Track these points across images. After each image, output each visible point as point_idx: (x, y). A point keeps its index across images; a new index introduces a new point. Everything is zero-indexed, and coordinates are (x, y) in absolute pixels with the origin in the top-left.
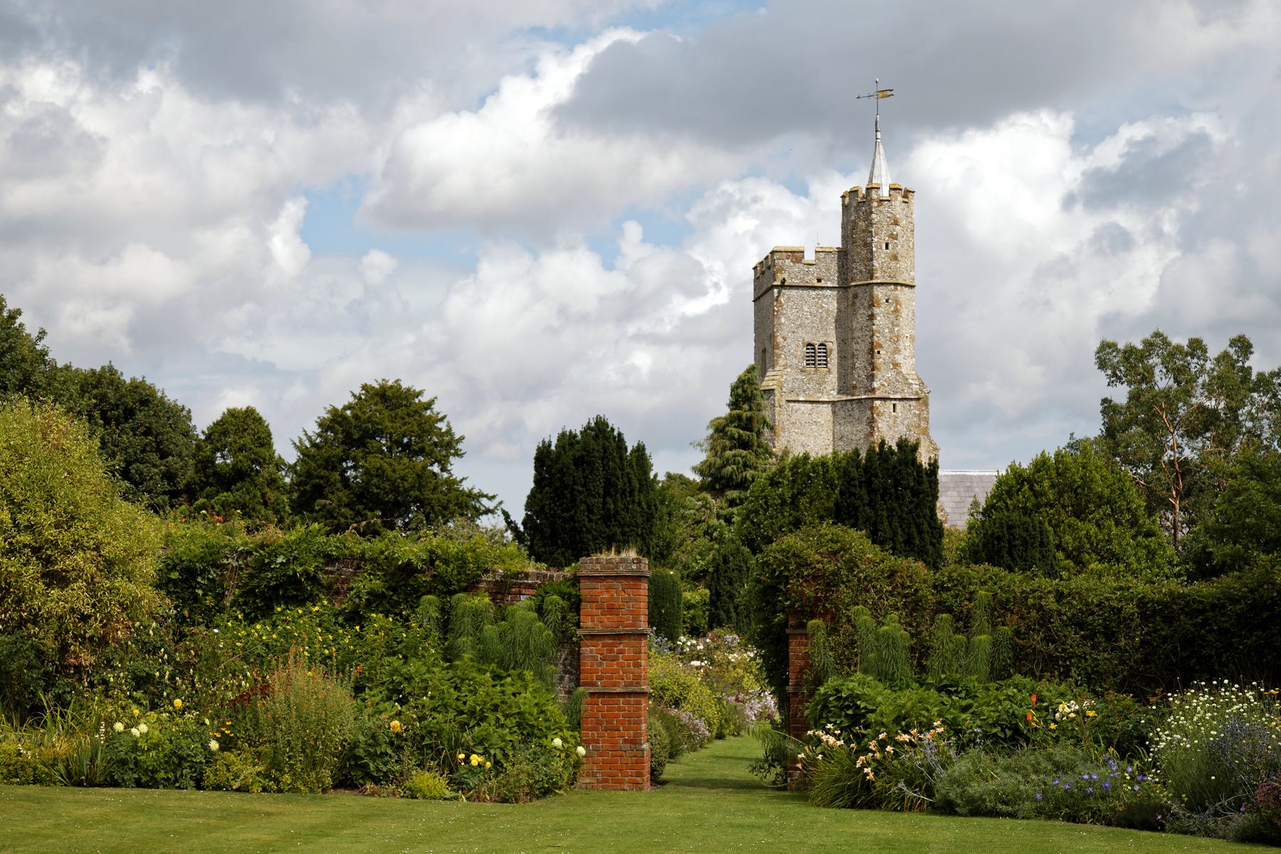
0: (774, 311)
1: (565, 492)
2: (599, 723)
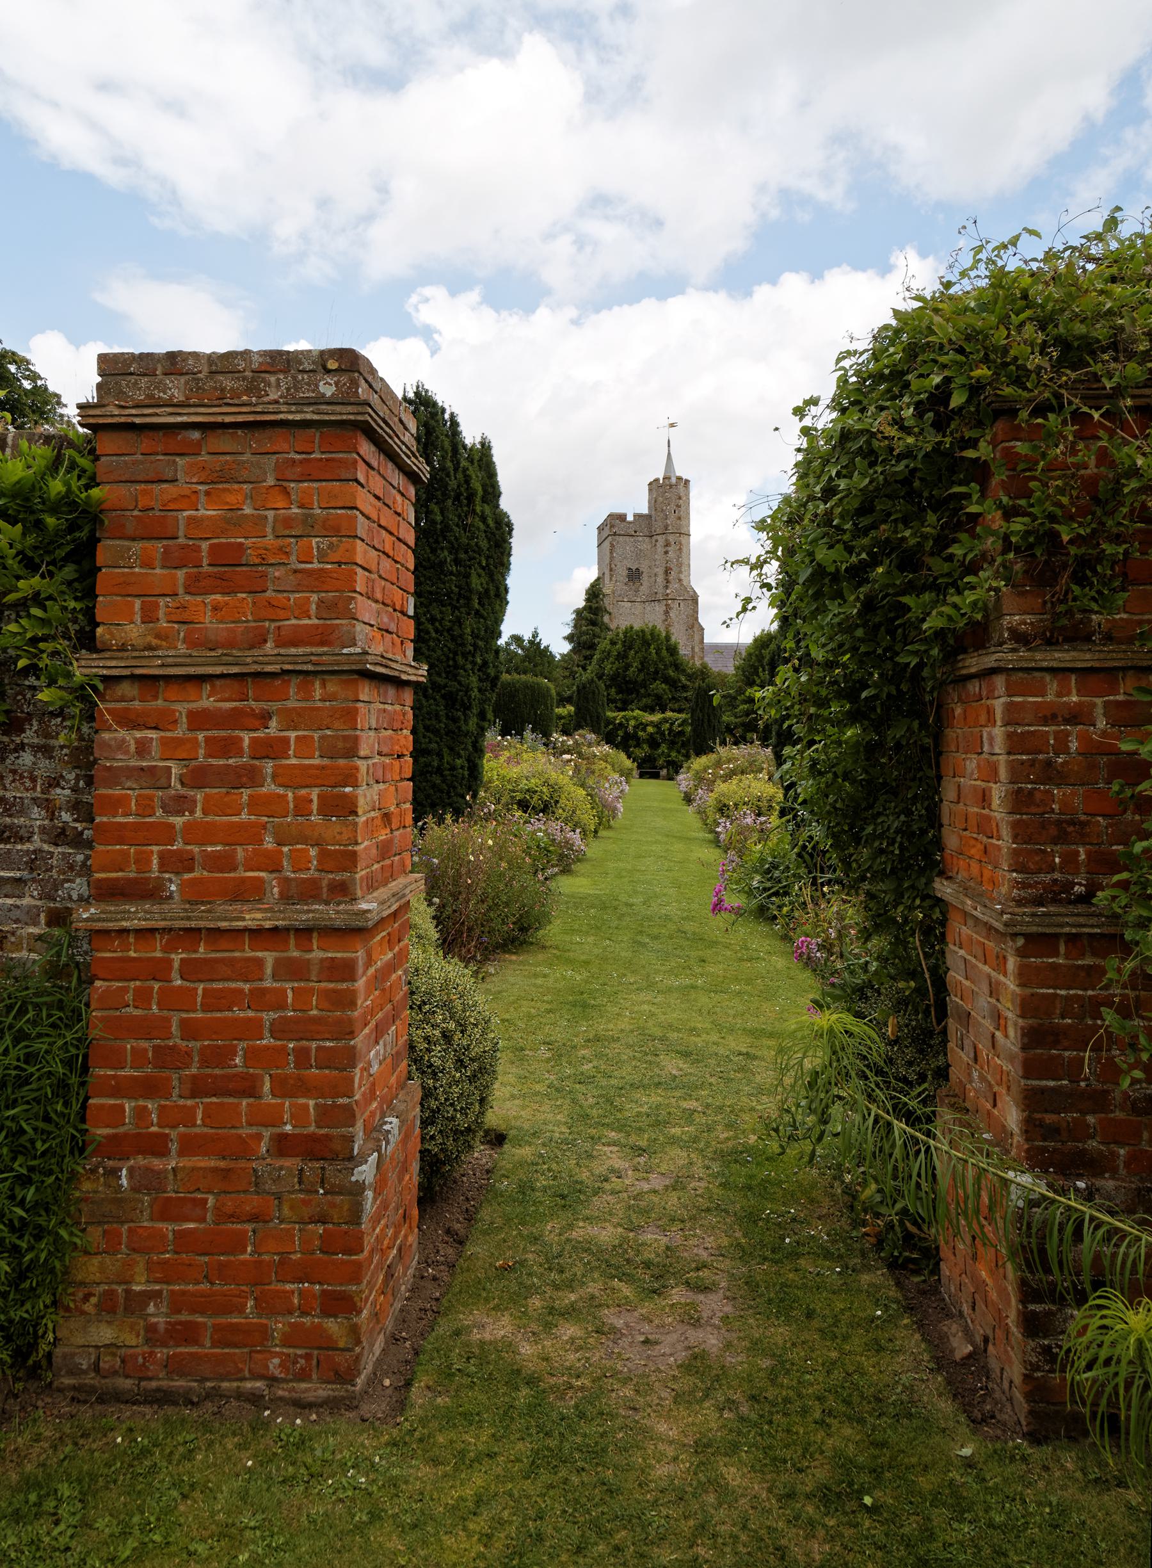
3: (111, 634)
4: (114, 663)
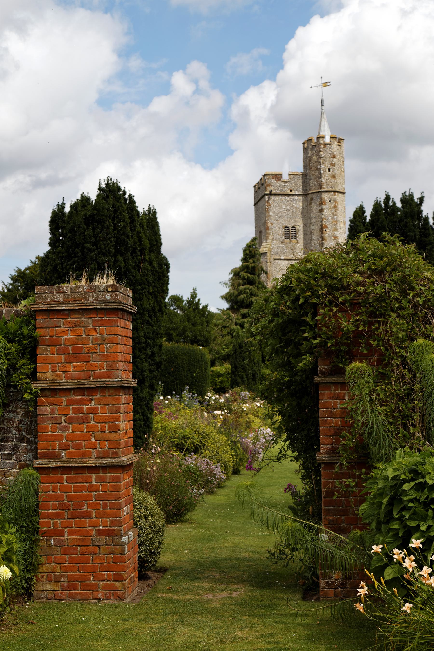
0: (266, 208)
1: (77, 250)
2: (64, 508)
3: (42, 375)
4: (44, 385)
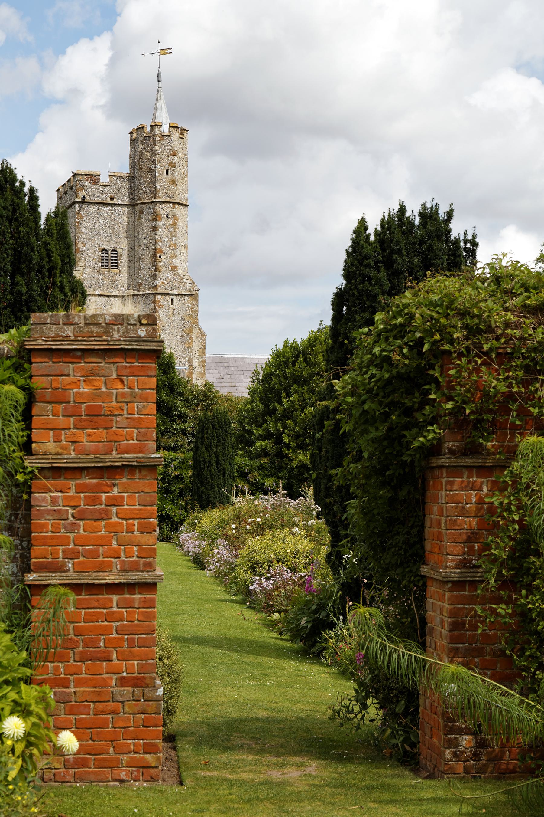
0: (76, 222)
2: (70, 645)
3: (39, 447)
